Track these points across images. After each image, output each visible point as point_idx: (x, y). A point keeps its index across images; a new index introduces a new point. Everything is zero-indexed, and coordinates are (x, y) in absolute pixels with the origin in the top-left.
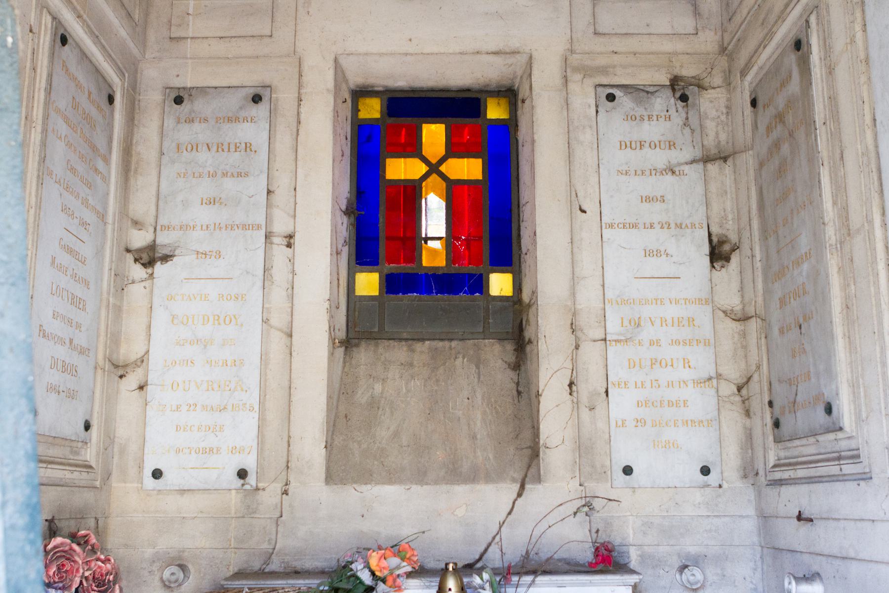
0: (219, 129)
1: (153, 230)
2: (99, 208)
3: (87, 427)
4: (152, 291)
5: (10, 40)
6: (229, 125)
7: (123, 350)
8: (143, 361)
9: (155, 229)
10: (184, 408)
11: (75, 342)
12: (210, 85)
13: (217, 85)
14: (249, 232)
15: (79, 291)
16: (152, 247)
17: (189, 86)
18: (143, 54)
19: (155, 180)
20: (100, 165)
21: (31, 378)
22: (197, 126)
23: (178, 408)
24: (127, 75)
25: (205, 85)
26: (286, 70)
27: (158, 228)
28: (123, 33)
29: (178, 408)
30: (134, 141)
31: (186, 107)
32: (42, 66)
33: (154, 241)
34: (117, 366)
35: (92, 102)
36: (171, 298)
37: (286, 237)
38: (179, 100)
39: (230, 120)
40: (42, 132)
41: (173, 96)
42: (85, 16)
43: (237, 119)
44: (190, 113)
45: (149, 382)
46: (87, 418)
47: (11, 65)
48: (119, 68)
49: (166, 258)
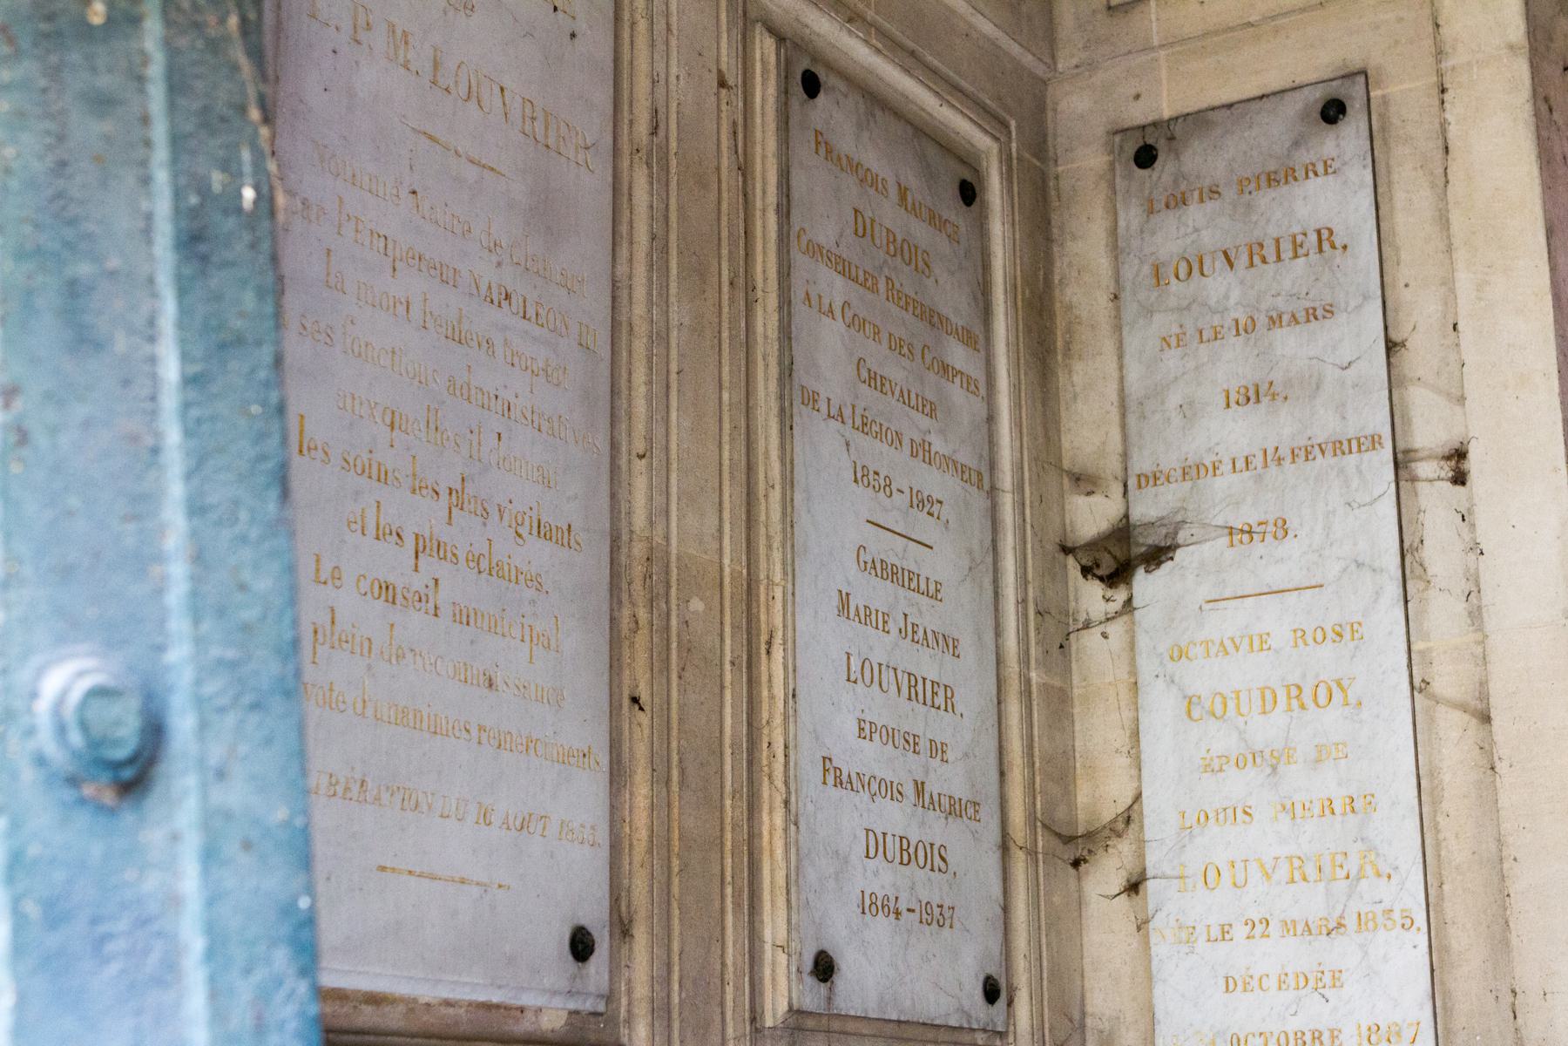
0: (1249, 206)
1: (1121, 489)
2: (965, 457)
3: (991, 992)
4: (1132, 646)
5: (248, 194)
6: (1272, 193)
7: (1083, 797)
8: (1128, 821)
9: (1125, 486)
10: (1240, 932)
11: (933, 787)
12: (1217, 103)
13: (1235, 97)
14: (1352, 459)
15: (928, 665)
16: (1123, 531)
17: (1167, 114)
18: (1052, 66)
19: (1112, 367)
20: (958, 355)
21: (304, 903)
22: (1195, 213)
23: (1225, 932)
24: (1013, 124)
25: (1204, 105)
26: (1400, 20)
27: (1132, 482)
28: (987, 28)
29: (1225, 932)
30: (1056, 279)
31: (1165, 168)
32: (764, 157)
33: (1126, 516)
34: (1069, 840)
35: (914, 210)
36: (1180, 654)
37: (1448, 458)
38: (1145, 157)
39: (1272, 180)
40: (780, 308)
41: (1131, 149)
42: (870, 14)
43: (1290, 175)
44: (1176, 182)
45: (1150, 873)
46: (993, 970)
47: (253, 246)
49: (1157, 556)
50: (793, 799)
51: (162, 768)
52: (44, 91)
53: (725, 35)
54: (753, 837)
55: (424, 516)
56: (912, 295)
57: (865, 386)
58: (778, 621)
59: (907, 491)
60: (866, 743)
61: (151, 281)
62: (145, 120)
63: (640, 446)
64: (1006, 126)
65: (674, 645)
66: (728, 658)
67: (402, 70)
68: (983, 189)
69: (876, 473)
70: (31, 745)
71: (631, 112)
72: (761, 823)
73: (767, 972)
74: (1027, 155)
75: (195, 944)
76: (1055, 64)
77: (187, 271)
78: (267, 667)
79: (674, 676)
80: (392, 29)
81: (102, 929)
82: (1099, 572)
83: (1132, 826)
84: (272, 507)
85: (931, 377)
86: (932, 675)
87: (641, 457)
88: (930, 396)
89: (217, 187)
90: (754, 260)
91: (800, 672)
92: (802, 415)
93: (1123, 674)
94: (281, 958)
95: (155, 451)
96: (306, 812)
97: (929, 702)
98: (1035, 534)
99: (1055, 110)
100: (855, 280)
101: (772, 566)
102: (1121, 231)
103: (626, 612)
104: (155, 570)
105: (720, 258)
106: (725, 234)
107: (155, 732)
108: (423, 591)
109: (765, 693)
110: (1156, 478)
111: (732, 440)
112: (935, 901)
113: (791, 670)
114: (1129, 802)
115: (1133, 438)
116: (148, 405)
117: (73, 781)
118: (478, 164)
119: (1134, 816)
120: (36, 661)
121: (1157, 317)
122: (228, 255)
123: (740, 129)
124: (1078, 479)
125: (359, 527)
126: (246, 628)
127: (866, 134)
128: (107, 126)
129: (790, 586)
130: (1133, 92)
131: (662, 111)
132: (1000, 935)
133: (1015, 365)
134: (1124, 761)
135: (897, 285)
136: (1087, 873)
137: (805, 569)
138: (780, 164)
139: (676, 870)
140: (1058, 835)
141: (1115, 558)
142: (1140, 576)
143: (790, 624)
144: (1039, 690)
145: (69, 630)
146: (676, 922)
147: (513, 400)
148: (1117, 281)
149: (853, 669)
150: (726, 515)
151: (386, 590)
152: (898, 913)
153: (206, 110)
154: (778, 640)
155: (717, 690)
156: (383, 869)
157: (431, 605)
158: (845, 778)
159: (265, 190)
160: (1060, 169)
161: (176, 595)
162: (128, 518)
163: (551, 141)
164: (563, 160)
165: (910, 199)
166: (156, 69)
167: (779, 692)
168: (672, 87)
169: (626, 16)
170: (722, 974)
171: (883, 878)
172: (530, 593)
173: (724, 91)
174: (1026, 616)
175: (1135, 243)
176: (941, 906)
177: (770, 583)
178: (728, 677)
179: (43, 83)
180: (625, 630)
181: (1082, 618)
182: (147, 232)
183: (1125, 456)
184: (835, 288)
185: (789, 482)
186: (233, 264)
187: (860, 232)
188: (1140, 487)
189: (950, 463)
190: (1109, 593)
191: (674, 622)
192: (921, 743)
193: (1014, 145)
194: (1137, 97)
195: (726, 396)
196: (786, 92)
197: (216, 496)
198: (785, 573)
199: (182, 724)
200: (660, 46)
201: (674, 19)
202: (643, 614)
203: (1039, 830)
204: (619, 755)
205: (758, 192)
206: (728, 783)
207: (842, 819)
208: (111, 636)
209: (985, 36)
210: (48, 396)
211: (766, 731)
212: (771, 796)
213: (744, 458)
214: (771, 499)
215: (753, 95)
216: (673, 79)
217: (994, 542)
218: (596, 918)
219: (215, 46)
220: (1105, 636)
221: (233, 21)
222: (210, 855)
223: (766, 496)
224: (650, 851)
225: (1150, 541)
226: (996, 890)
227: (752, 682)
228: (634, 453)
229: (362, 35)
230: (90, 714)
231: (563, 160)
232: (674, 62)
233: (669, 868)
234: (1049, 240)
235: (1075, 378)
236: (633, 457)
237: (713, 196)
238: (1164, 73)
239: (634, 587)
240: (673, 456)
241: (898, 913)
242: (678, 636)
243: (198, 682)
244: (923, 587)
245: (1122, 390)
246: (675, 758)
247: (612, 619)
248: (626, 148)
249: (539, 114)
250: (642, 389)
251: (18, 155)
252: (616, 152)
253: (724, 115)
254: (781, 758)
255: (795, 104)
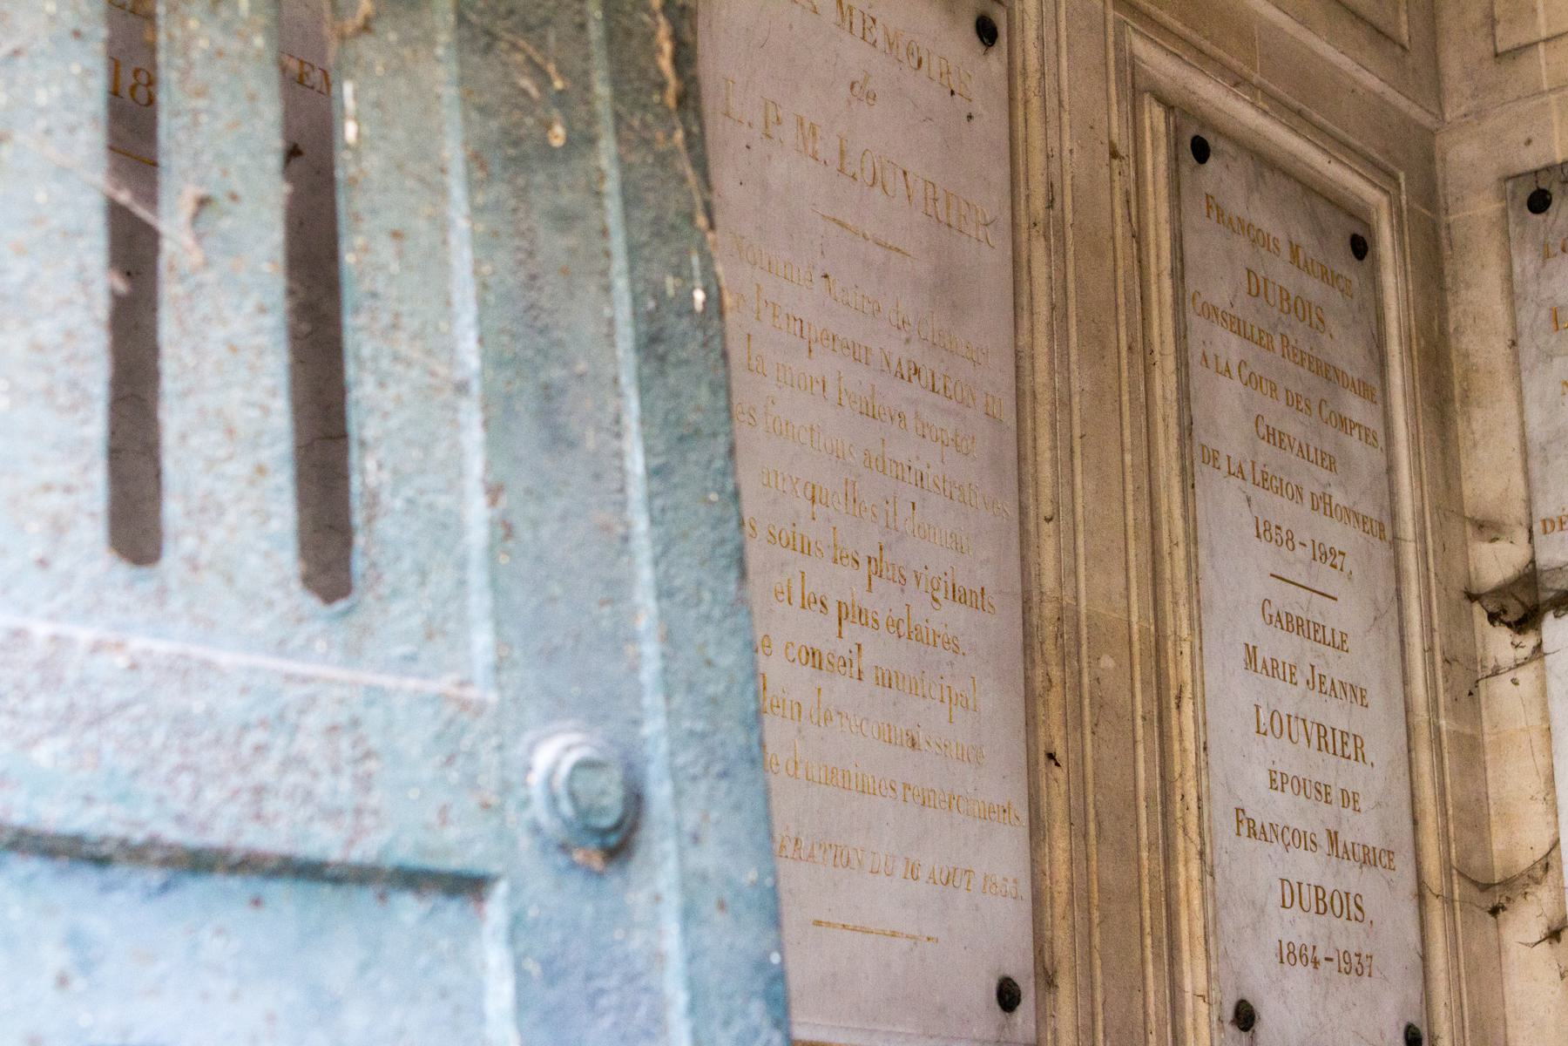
1: (1525, 535)
2: (1366, 508)
4: (1544, 691)
5: (699, 296)
7: (1498, 844)
8: (1547, 867)
9: (1530, 531)
11: (1346, 837)
15: (1336, 715)
16: (1530, 577)
19: (1513, 412)
20: (1356, 408)
21: (775, 958)
24: (1402, 176)
27: (1537, 528)
28: (1373, 82)
32: (1157, 223)
33: (1533, 561)
34: (1485, 887)
35: (1306, 268)
38: (1539, 202)
41: (1524, 193)
42: (1256, 78)
46: (1413, 1018)
47: (705, 345)
48: (1375, 165)
50: (1208, 850)
51: (644, 834)
52: (515, 210)
53: (1115, 108)
54: (1170, 887)
55: (845, 584)
56: (1307, 349)
57: (1264, 443)
58: (1187, 675)
59: (1309, 544)
60: (1277, 794)
61: (616, 380)
62: (604, 233)
63: (1047, 510)
64: (1395, 178)
65: (1087, 702)
66: (1139, 712)
67: (812, 162)
68: (1375, 242)
69: (1278, 528)
70: (527, 815)
71: (1028, 188)
72: (1177, 873)
73: (1189, 1021)
74: (1416, 206)
75: (679, 998)
76: (1443, 114)
77: (646, 371)
78: (735, 738)
79: (1088, 732)
80: (800, 122)
81: (599, 983)
82: (1507, 619)
83: (1550, 872)
84: (732, 587)
85: (1330, 431)
86: (1341, 725)
87: (1048, 520)
88: (1327, 448)
89: (671, 292)
90: (1150, 324)
91: (1210, 725)
92: (1202, 471)
93: (1535, 720)
94: (757, 1009)
95: (626, 539)
96: (774, 873)
97: (1339, 752)
98: (1439, 582)
99: (1444, 160)
100: (1250, 339)
101: (1179, 622)
102: (1517, 277)
103: (1039, 671)
104: (630, 650)
105: (1117, 323)
106: (1121, 300)
107: (635, 800)
108: (847, 656)
109: (1176, 747)
110: (1562, 523)
111: (1136, 500)
112: (1353, 950)
113: (1202, 723)
114: (1547, 848)
115: (1537, 485)
116: (619, 497)
117: (564, 848)
118: (885, 246)
119: (1553, 863)
120: (528, 737)
121: (1557, 361)
122: (684, 355)
123: (1133, 198)
124: (1481, 526)
125: (785, 597)
126: (714, 701)
127: (1256, 196)
128: (571, 241)
129: (1197, 642)
130: (1523, 138)
131: (1057, 186)
132: (1420, 982)
133: (1412, 416)
134: (1540, 807)
135: (1293, 343)
136: (1506, 920)
137: (1212, 624)
138: (1173, 230)
139: (1096, 921)
140: (1475, 883)
141: (1522, 603)
142: (1549, 618)
143: (1199, 679)
144: (1450, 739)
145: (557, 708)
146: (1098, 972)
147: (925, 471)
148: (1515, 328)
149: (1262, 720)
150: (1133, 574)
151: (813, 656)
152: (1316, 963)
153: (657, 220)
154: (1187, 694)
155: (1130, 745)
156: (818, 923)
157: (855, 669)
158: (1258, 828)
159: (714, 290)
160: (1451, 218)
161: (649, 672)
162: (602, 603)
163: (953, 221)
164: (965, 237)
165: (1302, 258)
166: (611, 186)
167: (1190, 745)
168: (1066, 160)
169: (1020, 95)
170: (1145, 1023)
171: (1300, 927)
172: (948, 655)
173: (1116, 162)
174: (1433, 663)
175: (1532, 288)
176: (1358, 955)
177: (1178, 639)
178: (1140, 732)
179: (512, 203)
180: (1039, 690)
181: (1491, 664)
182: (610, 337)
183: (1529, 502)
184: (1230, 347)
185: (1192, 539)
186: (687, 362)
187: (1254, 291)
188: (1545, 532)
189: (1351, 515)
190: (1518, 639)
191: (1086, 680)
192: (1333, 793)
193: (1404, 197)
194: (1529, 142)
195: (1128, 458)
196: (1177, 159)
197: (683, 578)
198: (1191, 628)
199: (659, 793)
200: (1053, 122)
201: (1065, 96)
202: (1055, 673)
203: (1455, 878)
204: (1037, 810)
205: (1153, 260)
206: (1144, 835)
207: (1256, 870)
208: (593, 712)
209: (1370, 91)
210: (528, 492)
211: (1178, 784)
212: (1186, 848)
213: (1147, 517)
214: (1176, 557)
215: (1144, 163)
216: (1066, 153)
217: (1398, 592)
218: (1020, 967)
219: (663, 160)
220: (1515, 682)
221: (679, 135)
222: (688, 915)
223: (1170, 554)
224: (1071, 902)
225: (1558, 586)
226: (1413, 936)
227: (1164, 736)
228: (1042, 517)
229: (773, 130)
230: (578, 785)
231: (965, 237)
232: (1066, 136)
233: (1090, 920)
234: (1442, 289)
235: (1475, 426)
236: (1042, 521)
237: (1109, 263)
238: (1555, 118)
239: (1046, 646)
240: (1079, 517)
241: (1316, 963)
242: (1091, 693)
243: (672, 754)
244: (1329, 638)
245: (1523, 437)
246: (1092, 812)
247: (1026, 678)
248: (1023, 222)
249: (940, 193)
250: (1048, 455)
251: (494, 273)
252: (1014, 225)
253: (1117, 185)
254: (1193, 805)
255: (1185, 170)
